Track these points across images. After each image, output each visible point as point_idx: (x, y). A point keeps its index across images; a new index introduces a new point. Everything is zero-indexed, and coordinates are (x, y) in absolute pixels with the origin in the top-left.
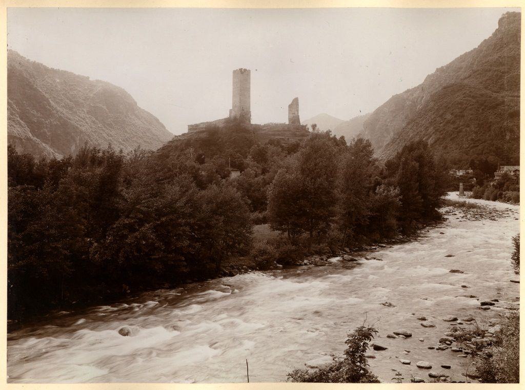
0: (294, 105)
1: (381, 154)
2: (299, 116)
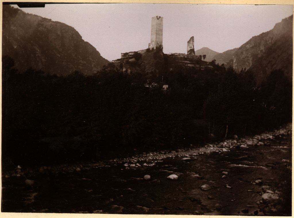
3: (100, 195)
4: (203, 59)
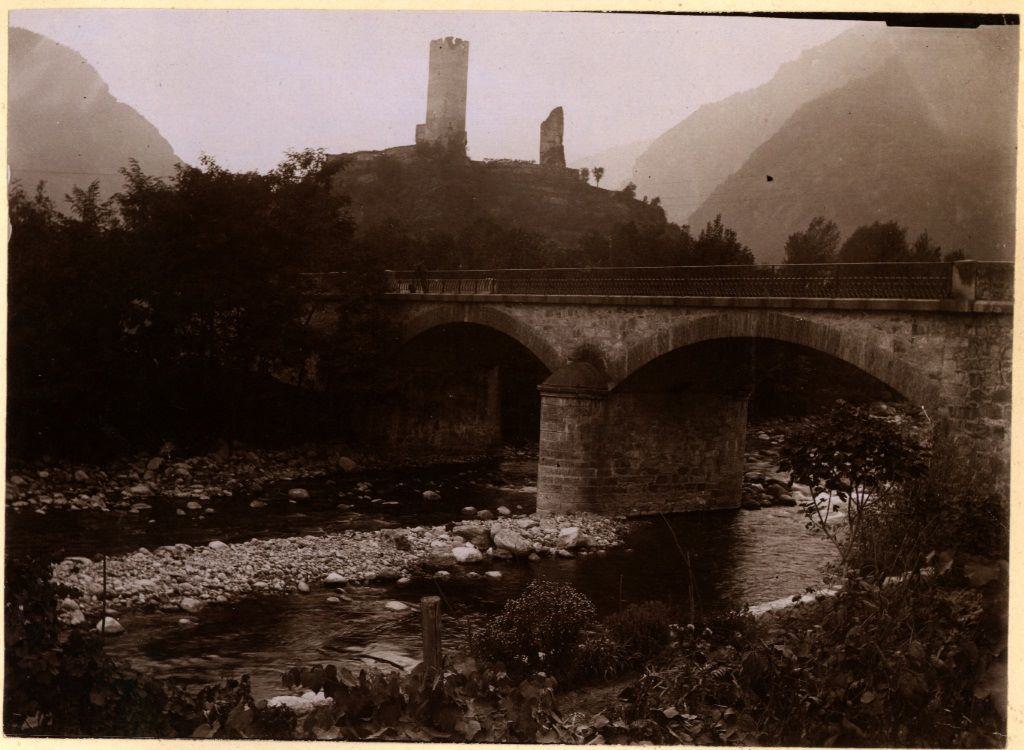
0: (554, 124)
1: (695, 234)
2: (562, 147)
3: (227, 637)
4: (592, 181)
